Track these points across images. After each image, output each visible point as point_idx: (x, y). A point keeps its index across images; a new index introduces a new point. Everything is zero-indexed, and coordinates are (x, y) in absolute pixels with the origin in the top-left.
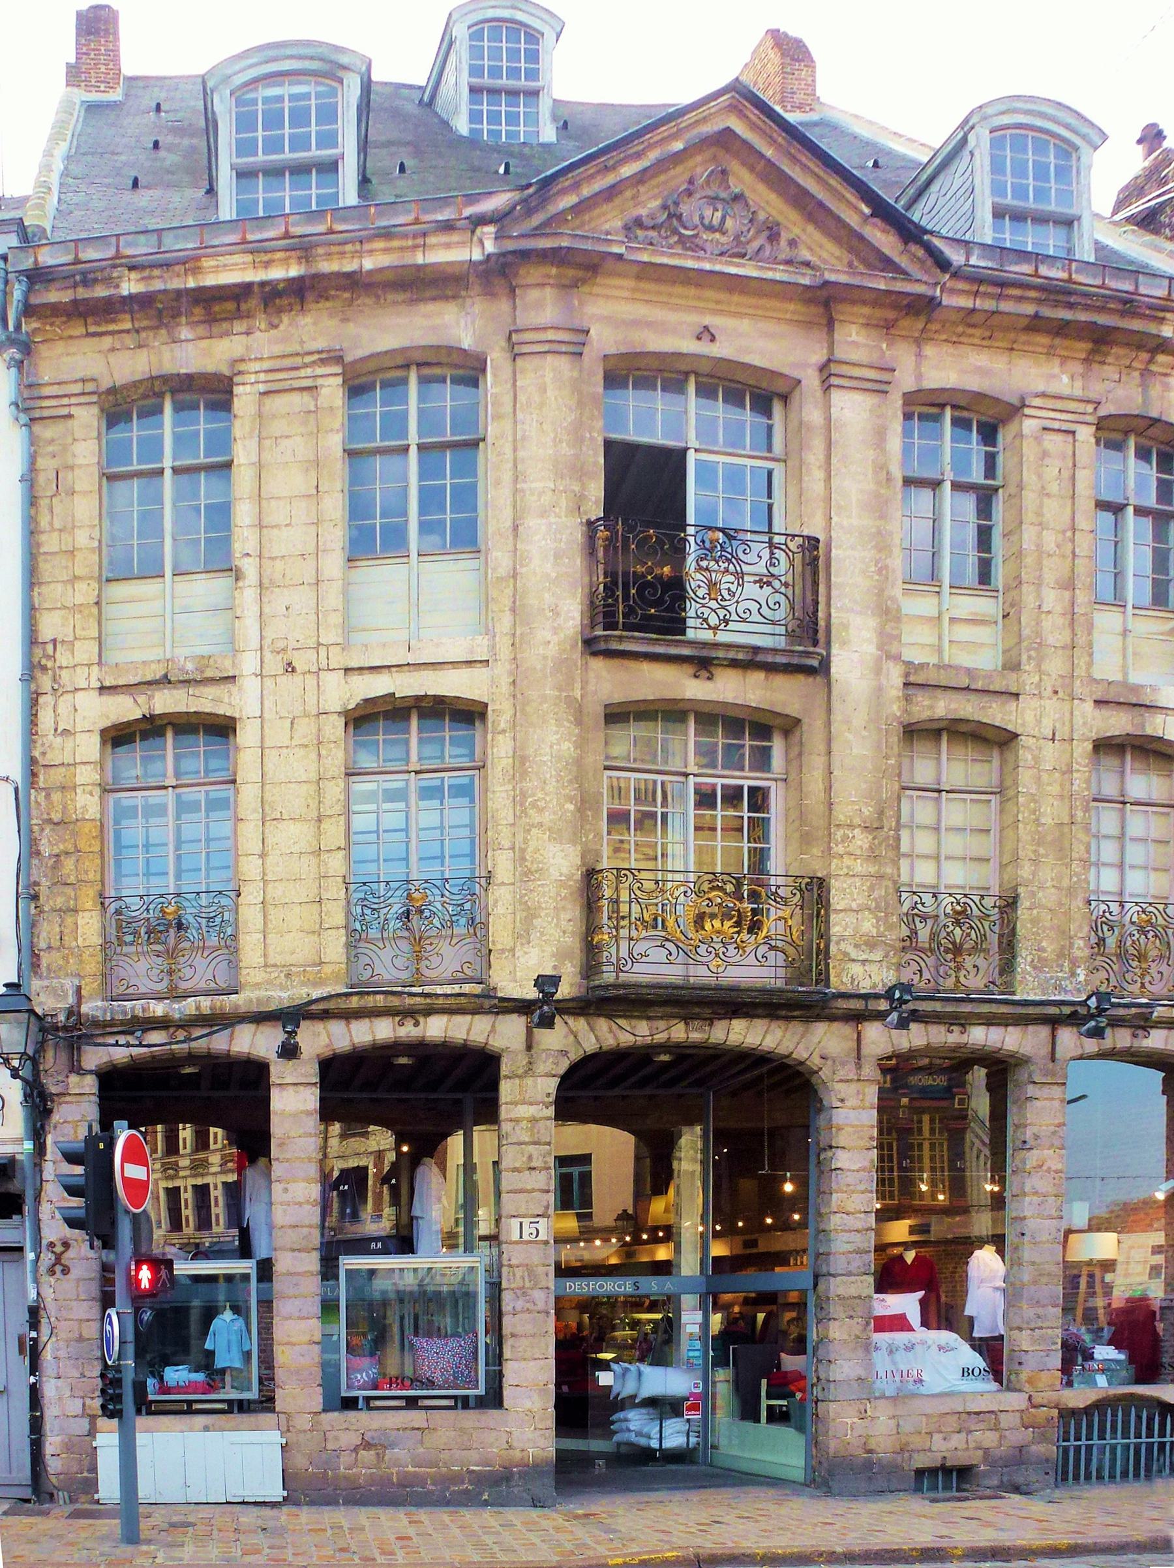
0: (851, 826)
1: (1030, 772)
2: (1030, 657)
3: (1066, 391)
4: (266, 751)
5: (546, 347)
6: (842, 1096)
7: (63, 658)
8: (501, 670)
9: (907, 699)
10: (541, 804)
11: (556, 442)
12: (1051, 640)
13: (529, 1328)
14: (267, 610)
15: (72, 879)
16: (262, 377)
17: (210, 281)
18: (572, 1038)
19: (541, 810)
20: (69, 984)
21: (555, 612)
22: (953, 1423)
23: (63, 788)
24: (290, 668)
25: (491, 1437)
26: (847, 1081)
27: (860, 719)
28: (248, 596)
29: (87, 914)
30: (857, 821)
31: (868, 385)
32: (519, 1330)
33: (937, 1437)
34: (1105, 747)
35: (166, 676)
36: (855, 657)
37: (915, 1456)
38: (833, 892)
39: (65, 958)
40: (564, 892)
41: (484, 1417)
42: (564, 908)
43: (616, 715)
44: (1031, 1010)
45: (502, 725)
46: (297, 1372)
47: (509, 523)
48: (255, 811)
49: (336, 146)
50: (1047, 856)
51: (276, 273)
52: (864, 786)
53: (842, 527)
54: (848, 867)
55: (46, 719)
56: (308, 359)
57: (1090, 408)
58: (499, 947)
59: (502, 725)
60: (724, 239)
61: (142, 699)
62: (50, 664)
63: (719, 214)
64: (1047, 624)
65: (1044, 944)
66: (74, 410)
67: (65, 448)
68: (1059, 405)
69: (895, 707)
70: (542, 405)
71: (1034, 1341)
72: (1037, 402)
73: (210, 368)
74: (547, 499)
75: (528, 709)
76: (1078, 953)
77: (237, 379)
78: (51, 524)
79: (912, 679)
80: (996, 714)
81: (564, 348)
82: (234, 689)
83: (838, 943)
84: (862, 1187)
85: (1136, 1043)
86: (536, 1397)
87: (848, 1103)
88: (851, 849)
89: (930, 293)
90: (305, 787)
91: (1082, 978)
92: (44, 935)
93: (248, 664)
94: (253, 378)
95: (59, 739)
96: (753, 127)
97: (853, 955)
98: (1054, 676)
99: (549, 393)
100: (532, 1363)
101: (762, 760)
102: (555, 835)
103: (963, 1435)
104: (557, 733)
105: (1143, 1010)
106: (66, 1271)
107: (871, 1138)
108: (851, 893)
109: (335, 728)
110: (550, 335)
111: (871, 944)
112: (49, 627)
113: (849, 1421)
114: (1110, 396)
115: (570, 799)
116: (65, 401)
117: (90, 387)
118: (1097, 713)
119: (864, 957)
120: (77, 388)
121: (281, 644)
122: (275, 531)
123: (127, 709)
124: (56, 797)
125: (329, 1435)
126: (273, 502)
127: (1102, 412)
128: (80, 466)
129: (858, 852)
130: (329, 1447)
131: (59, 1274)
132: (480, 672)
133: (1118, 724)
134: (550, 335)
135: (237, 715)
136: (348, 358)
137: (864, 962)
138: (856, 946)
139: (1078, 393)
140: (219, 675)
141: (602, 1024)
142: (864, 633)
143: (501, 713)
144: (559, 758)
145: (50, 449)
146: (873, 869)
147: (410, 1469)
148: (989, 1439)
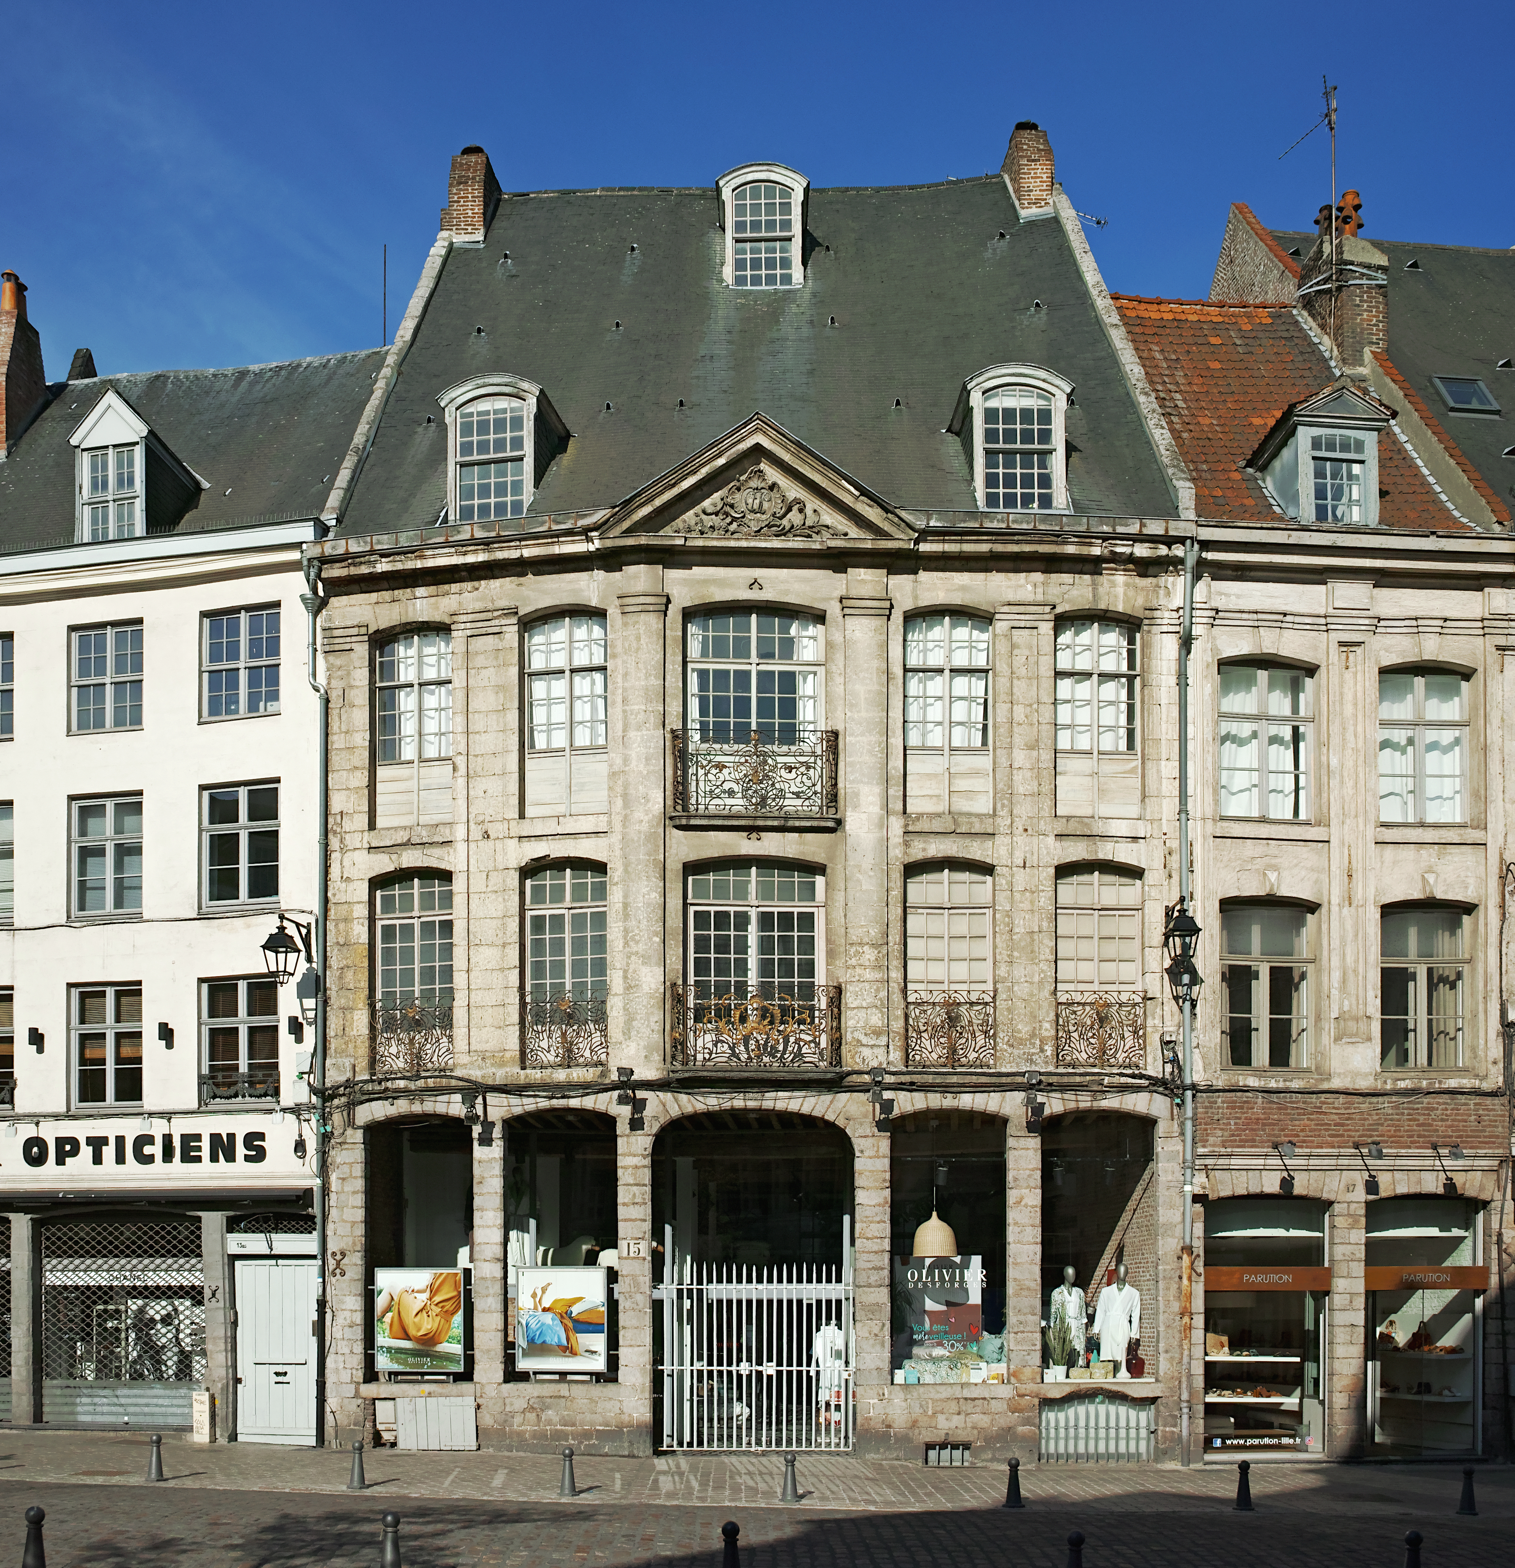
0: (861, 944)
1: (1005, 894)
2: (1003, 806)
3: (1030, 598)
4: (471, 896)
5: (640, 608)
6: (862, 1147)
7: (347, 825)
8: (615, 838)
9: (906, 844)
10: (637, 938)
11: (647, 676)
12: (1021, 790)
13: (635, 1322)
14: (471, 793)
15: (351, 986)
16: (468, 625)
17: (430, 563)
18: (661, 1107)
19: (637, 942)
20: (347, 1062)
21: (646, 798)
22: (953, 1406)
23: (346, 920)
24: (487, 836)
25: (609, 1405)
26: (865, 1137)
27: (867, 863)
28: (461, 782)
29: (359, 1012)
30: (866, 940)
31: (873, 612)
32: (627, 1324)
33: (941, 1418)
34: (1064, 871)
35: (409, 840)
36: (864, 817)
37: (923, 1432)
38: (848, 994)
39: (346, 1043)
40: (652, 1002)
41: (605, 1390)
42: (652, 1013)
43: (692, 868)
44: (1004, 1080)
45: (616, 880)
46: (488, 1351)
47: (620, 733)
48: (464, 939)
49: (522, 450)
50: (1020, 958)
51: (470, 559)
52: (871, 913)
53: (853, 720)
54: (859, 975)
55: (335, 872)
56: (496, 614)
57: (1047, 609)
58: (614, 1040)
59: (616, 880)
60: (764, 517)
61: (394, 857)
62: (338, 830)
63: (757, 501)
64: (1018, 777)
65: (1020, 1027)
66: (354, 646)
67: (349, 674)
68: (1021, 609)
69: (897, 851)
70: (638, 649)
71: (1018, 1343)
72: (1006, 609)
73: (437, 618)
74: (641, 717)
75: (629, 869)
76: (1045, 1034)
77: (453, 627)
78: (340, 728)
79: (910, 828)
80: (976, 851)
81: (651, 608)
82: (451, 851)
83: (852, 1033)
84: (878, 1219)
85: (1095, 1104)
86: (638, 1375)
87: (866, 1154)
88: (861, 962)
89: (906, 546)
90: (495, 922)
91: (1049, 1053)
92: (333, 1026)
93: (460, 832)
94: (463, 626)
95: (344, 885)
96: (774, 441)
97: (864, 1042)
98: (1024, 818)
99: (642, 642)
100: (636, 1349)
101: (809, 891)
102: (646, 960)
103: (962, 1416)
104: (647, 886)
105: (1096, 1078)
106: (343, 1274)
107: (884, 1180)
108: (862, 994)
109: (514, 879)
110: (642, 600)
111: (877, 1033)
112: (336, 805)
113: (872, 1401)
114: (1066, 596)
115: (656, 934)
116: (348, 640)
117: (363, 630)
118: (1058, 844)
119: (872, 1043)
120: (355, 631)
121: (481, 818)
122: (478, 736)
123: (385, 864)
124: (342, 926)
125: (507, 1401)
126: (476, 715)
127: (1059, 610)
128: (357, 687)
129: (867, 963)
130: (507, 1409)
131: (338, 1276)
132: (602, 841)
133: (1077, 852)
134: (642, 600)
135: (452, 869)
136: (521, 613)
137: (872, 1046)
138: (866, 1035)
139: (1040, 598)
140: (441, 840)
141: (683, 1098)
142: (871, 798)
143: (615, 871)
144: (649, 905)
145: (340, 673)
146: (878, 975)
147: (559, 1427)
148: (984, 1421)
